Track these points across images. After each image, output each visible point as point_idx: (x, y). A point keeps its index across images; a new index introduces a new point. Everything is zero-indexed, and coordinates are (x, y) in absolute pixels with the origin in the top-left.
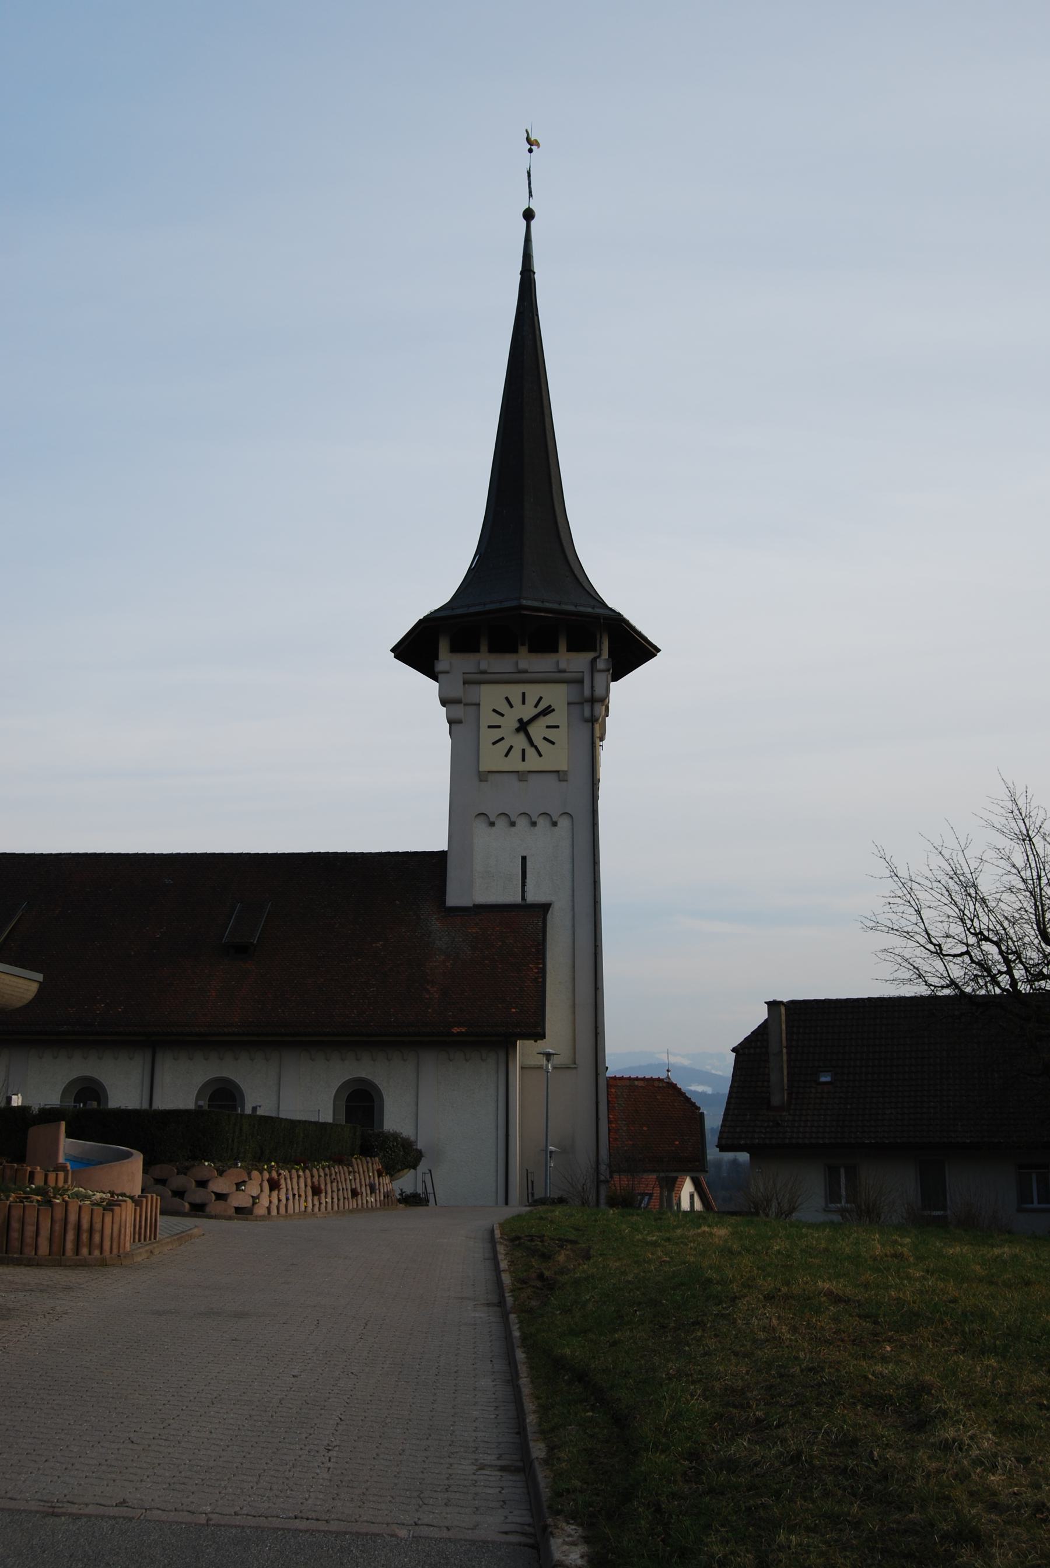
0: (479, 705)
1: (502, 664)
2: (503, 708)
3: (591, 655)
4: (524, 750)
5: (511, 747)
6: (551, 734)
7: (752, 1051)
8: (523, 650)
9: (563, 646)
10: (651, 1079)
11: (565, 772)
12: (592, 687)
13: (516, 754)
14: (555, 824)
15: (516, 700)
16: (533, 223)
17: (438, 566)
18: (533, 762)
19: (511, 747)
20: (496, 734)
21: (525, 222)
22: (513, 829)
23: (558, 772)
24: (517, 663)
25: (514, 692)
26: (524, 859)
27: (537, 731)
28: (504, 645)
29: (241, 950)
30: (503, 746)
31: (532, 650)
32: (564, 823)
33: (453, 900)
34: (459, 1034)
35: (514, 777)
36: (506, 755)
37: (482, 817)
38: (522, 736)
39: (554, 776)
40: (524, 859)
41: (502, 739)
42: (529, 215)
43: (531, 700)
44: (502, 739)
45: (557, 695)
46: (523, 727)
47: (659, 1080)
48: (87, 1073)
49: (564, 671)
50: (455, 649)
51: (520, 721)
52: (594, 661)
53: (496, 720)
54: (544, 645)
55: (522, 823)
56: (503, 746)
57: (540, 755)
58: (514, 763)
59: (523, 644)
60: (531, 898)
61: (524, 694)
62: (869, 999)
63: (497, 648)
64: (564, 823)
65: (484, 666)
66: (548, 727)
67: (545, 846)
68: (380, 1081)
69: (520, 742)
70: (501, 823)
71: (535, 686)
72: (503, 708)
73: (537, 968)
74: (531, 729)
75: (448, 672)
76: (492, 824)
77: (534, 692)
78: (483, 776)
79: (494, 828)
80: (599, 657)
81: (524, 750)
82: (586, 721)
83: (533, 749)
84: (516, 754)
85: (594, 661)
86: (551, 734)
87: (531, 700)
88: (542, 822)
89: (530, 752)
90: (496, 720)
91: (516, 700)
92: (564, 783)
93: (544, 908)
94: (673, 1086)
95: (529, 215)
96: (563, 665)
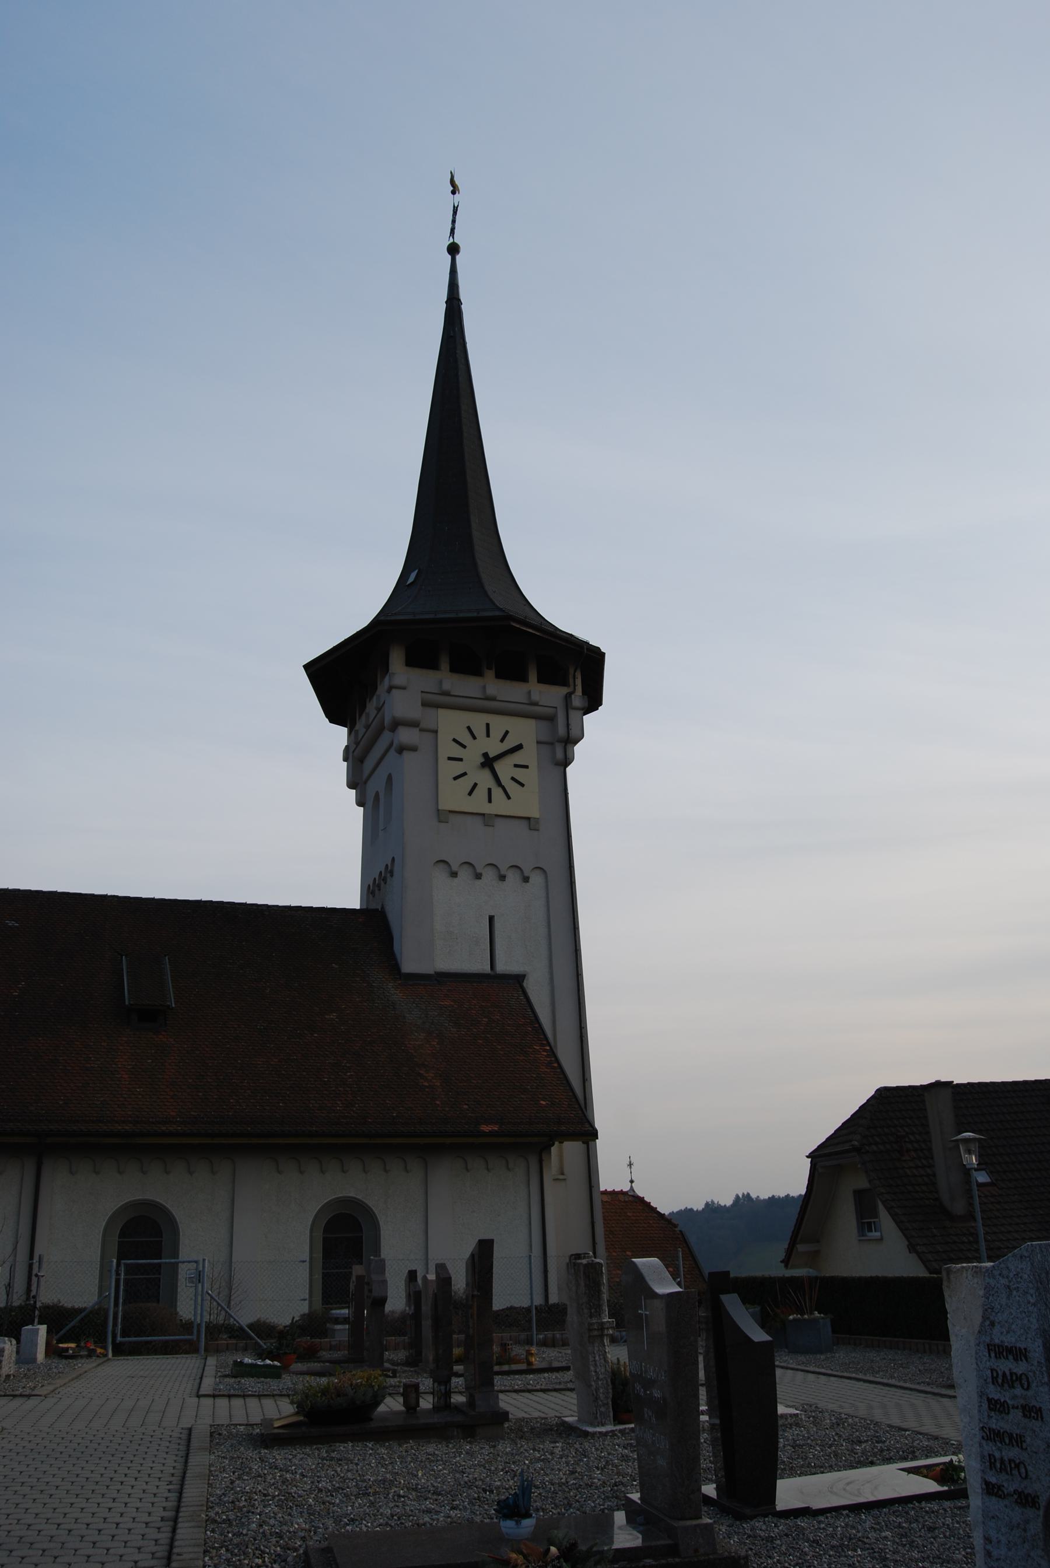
0: (436, 732)
1: (466, 686)
2: (466, 738)
3: (564, 691)
4: (490, 790)
5: (475, 785)
6: (519, 774)
7: (875, 1148)
8: (490, 674)
9: (533, 676)
10: (613, 1192)
11: (537, 820)
12: (568, 725)
13: (481, 793)
14: (526, 880)
15: (480, 731)
16: (459, 258)
17: (358, 583)
18: (500, 805)
19: (475, 785)
20: (457, 768)
21: (450, 257)
22: (478, 882)
23: (529, 819)
24: (484, 687)
25: (478, 721)
26: (491, 919)
27: (504, 769)
28: (466, 665)
29: (150, 1016)
30: (466, 783)
31: (499, 676)
32: (536, 879)
33: (409, 966)
34: (491, 1134)
35: (479, 820)
36: (470, 794)
37: (442, 865)
38: (486, 774)
39: (525, 823)
40: (491, 919)
41: (465, 774)
42: (453, 250)
43: (496, 733)
44: (465, 774)
45: (524, 731)
46: (488, 762)
47: (622, 1192)
48: (150, 1195)
49: (536, 704)
50: (411, 662)
51: (485, 755)
52: (568, 697)
53: (457, 752)
54: (513, 673)
55: (489, 875)
56: (466, 783)
57: (509, 798)
58: (478, 803)
59: (490, 668)
60: (501, 967)
61: (488, 725)
62: (1025, 1082)
63: (460, 667)
64: (536, 879)
65: (446, 686)
66: (516, 766)
67: (515, 904)
68: (374, 1202)
69: (485, 779)
70: (465, 874)
71: (457, 726)
72: (466, 738)
73: (545, 1050)
74: (498, 766)
75: (404, 688)
76: (454, 875)
77: (499, 724)
78: (443, 816)
79: (456, 880)
80: (573, 692)
81: (490, 790)
82: (557, 764)
83: (500, 790)
84: (481, 793)
85: (568, 697)
86: (519, 774)
87: (496, 733)
88: (512, 877)
89: (497, 793)
90: (457, 752)
91: (480, 731)
92: (536, 833)
93: (518, 980)
94: (641, 1200)
95: (453, 250)
96: (535, 697)
